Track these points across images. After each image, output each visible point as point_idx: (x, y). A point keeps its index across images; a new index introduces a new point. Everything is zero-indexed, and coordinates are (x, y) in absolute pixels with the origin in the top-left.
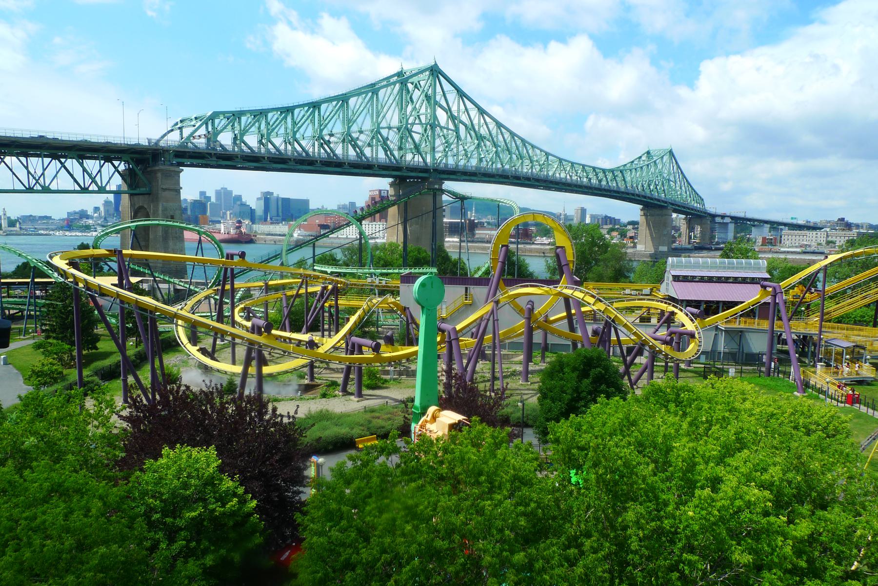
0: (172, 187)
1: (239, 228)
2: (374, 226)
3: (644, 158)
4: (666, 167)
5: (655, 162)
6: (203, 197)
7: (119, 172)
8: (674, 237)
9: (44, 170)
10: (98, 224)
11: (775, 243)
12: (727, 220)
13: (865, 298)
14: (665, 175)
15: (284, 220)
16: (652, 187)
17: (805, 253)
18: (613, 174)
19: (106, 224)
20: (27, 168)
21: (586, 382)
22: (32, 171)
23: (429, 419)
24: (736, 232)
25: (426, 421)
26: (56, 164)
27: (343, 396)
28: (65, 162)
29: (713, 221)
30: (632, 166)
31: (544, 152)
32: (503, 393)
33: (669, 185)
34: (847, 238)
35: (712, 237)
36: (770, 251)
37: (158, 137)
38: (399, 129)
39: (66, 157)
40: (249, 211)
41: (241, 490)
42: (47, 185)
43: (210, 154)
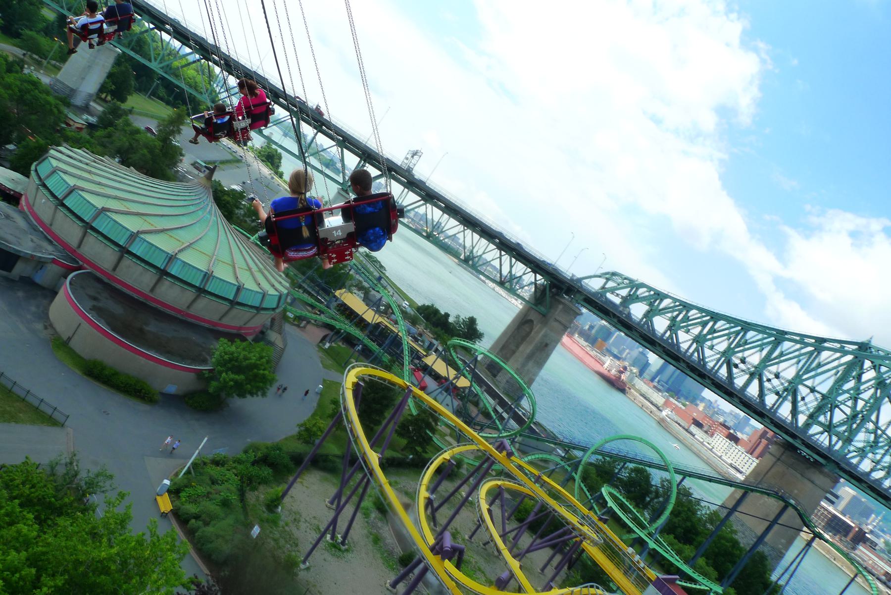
1: (621, 372)
2: (747, 458)
7: (536, 284)
15: (668, 390)
38: (824, 397)
40: (645, 362)
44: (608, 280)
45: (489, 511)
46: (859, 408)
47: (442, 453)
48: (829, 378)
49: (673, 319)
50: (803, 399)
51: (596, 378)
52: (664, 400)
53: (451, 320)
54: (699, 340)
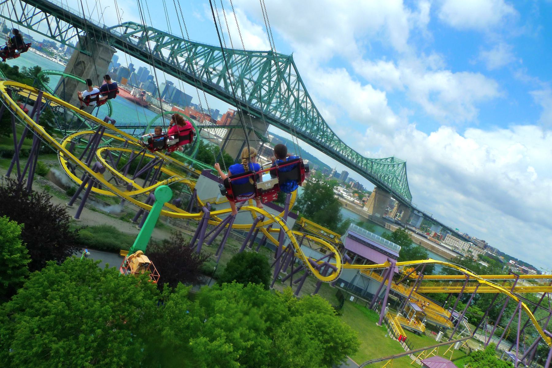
0: (106, 58)
1: (142, 95)
3: (389, 160)
4: (398, 170)
5: (394, 165)
6: (131, 67)
8: (387, 211)
9: (34, 15)
10: (59, 55)
11: (441, 238)
12: (421, 215)
13: (444, 289)
14: (397, 175)
15: (172, 102)
16: (386, 178)
17: (453, 251)
18: (367, 161)
19: (64, 57)
20: (23, 10)
21: (249, 270)
22: (26, 13)
23: (135, 256)
24: (423, 223)
25: (134, 257)
26: (42, 15)
27: (133, 223)
28: (49, 16)
29: (412, 212)
30: (379, 162)
31: (333, 132)
32: (206, 258)
33: (396, 181)
34: (479, 253)
35: (408, 221)
36: (435, 242)
37: (110, 26)
38: (255, 83)
39: (51, 13)
41: (26, 251)
42: (31, 25)
43: (137, 50)
44: (127, 27)
45: (106, 161)
46: (272, 86)
47: (66, 138)
48: (257, 72)
49: (172, 48)
50: (246, 86)
51: (128, 101)
52: (171, 108)
53: (20, 70)
54: (188, 61)
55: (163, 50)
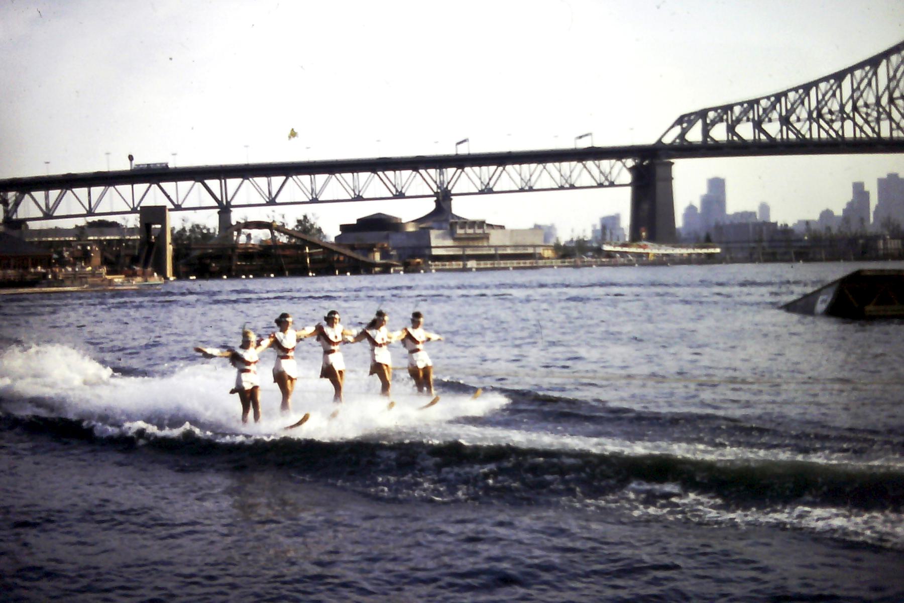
20: (560, 171)
55: (739, 129)
